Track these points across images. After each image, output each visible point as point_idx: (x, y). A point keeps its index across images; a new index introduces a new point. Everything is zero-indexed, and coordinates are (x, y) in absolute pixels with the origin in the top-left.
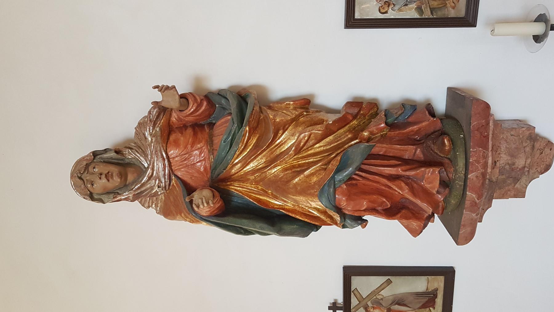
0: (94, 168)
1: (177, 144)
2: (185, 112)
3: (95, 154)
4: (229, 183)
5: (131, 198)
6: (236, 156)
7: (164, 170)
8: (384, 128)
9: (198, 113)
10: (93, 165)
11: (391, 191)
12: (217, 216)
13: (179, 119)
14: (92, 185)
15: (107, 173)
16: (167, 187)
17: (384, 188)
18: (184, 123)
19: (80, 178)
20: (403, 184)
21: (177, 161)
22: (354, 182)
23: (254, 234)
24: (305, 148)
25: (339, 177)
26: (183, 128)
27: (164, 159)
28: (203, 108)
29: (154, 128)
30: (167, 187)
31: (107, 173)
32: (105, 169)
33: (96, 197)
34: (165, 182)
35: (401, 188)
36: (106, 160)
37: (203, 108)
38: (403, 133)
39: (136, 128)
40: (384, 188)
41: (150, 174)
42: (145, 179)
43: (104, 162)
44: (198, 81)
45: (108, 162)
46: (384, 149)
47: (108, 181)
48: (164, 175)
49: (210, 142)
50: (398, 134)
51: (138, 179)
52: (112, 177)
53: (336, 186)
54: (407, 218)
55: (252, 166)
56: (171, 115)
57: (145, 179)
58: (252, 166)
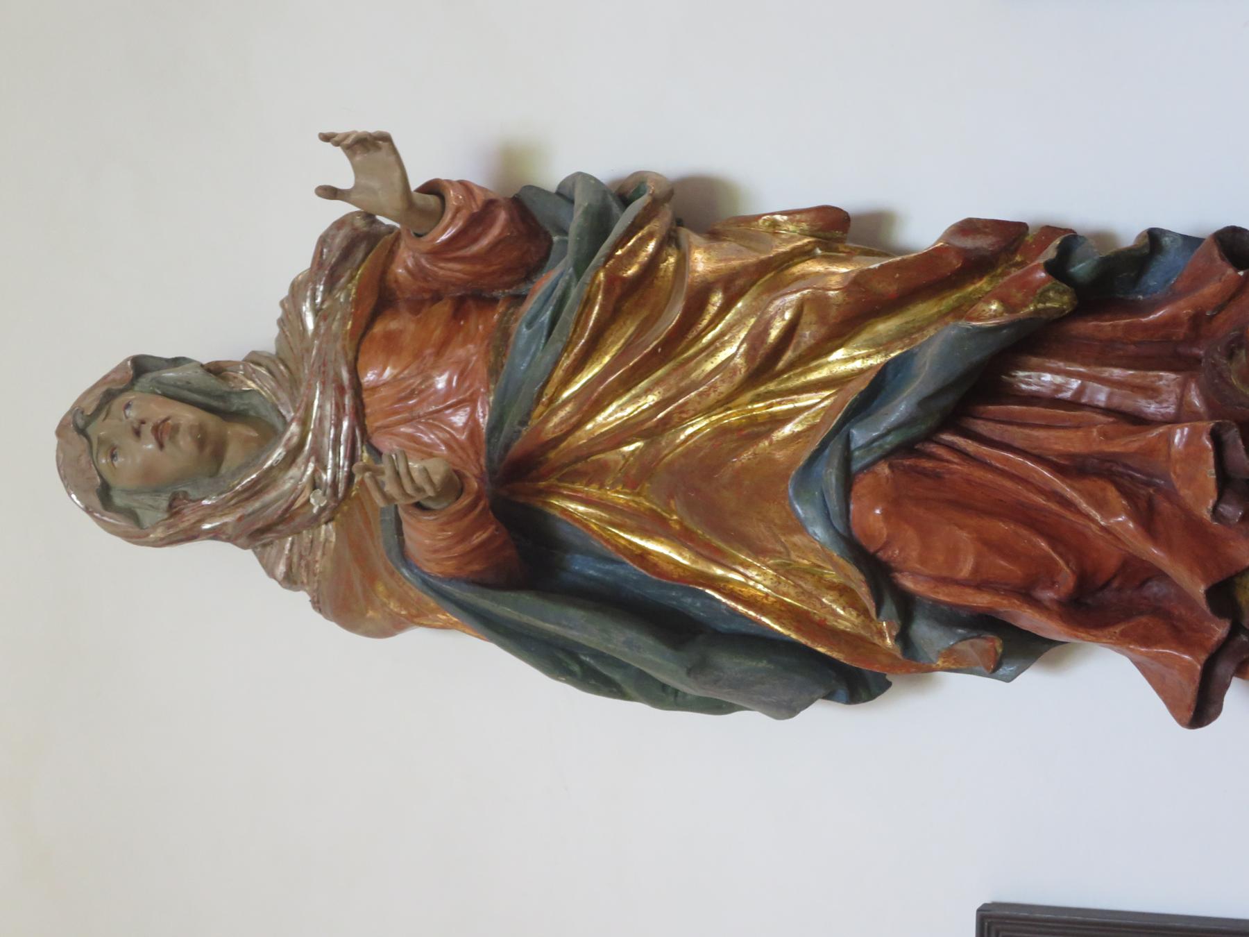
0: (128, 406)
1: (391, 345)
2: (428, 237)
3: (141, 366)
4: (542, 484)
5: (230, 530)
6: (559, 373)
7: (338, 425)
8: (1043, 281)
9: (475, 249)
10: (129, 397)
11: (1069, 515)
12: (480, 583)
13: (418, 273)
14: (113, 456)
15: (165, 449)
16: (341, 487)
17: (1041, 500)
18: (436, 286)
19: (82, 432)
20: (1112, 493)
21: (383, 399)
22: (928, 464)
23: (621, 694)
24: (789, 355)
25: (859, 436)
26: (427, 296)
27: (341, 390)
28: (495, 231)
29: (329, 290)
30: (341, 487)
31: (165, 449)
32: (159, 410)
33: (119, 500)
34: (336, 466)
35: (1101, 505)
36: (172, 390)
37: (495, 231)
38: (1146, 328)
39: (282, 304)
40: (1041, 500)
41: (295, 440)
42: (278, 454)
43: (165, 395)
44: (510, 158)
45: (174, 394)
46: (1075, 384)
47: (161, 446)
48: (337, 440)
49: (501, 341)
50: (1129, 329)
51: (258, 457)
52: (172, 438)
53: (856, 466)
54: (1146, 640)
55: (613, 415)
56: (391, 253)
57: (278, 454)
58: (613, 415)
